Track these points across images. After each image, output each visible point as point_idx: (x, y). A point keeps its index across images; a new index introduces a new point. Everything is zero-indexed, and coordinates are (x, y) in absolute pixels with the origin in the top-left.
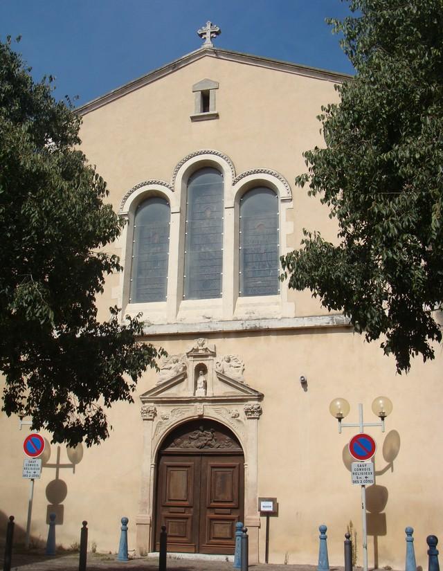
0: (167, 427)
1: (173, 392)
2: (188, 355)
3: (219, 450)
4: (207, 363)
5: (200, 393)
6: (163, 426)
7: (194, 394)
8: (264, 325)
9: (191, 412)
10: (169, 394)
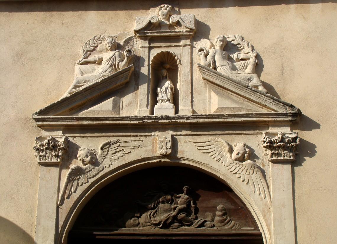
0: (91, 181)
1: (104, 108)
2: (141, 33)
3: (112, 168)
4: (181, 52)
5: (164, 109)
6: (83, 179)
7: (152, 112)
8: (189, 80)
9: (153, 147)
10: (98, 112)
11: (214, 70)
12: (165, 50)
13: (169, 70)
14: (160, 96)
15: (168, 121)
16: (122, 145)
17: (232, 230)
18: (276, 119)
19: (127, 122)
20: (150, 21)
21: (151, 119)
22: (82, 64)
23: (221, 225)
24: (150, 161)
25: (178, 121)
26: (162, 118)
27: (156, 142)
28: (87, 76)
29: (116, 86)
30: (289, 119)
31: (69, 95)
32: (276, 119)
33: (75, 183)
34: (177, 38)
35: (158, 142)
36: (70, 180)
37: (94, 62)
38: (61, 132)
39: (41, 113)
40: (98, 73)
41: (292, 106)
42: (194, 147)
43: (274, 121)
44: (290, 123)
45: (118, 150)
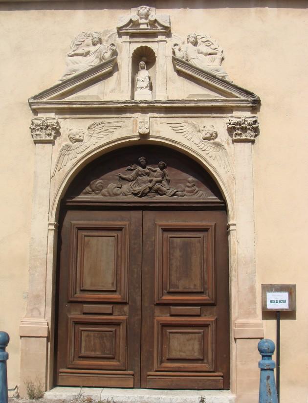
2: (121, 32)
5: (143, 95)
9: (127, 129)
11: (186, 62)
12: (144, 45)
13: (147, 63)
14: (139, 84)
15: (146, 105)
16: (107, 125)
17: (200, 199)
18: (239, 104)
19: (111, 106)
20: (131, 19)
21: (133, 102)
22: (71, 56)
23: (191, 194)
24: (131, 139)
25: (156, 105)
26: (141, 102)
27: (136, 123)
28: (76, 67)
29: (105, 70)
30: (251, 105)
31: (61, 82)
32: (239, 104)
33: (66, 157)
34: (154, 35)
35: (138, 123)
36: (62, 155)
37: (81, 55)
38: (54, 114)
39: (35, 97)
40: (84, 64)
41: (251, 94)
42: (167, 127)
43: (238, 107)
44: (251, 109)
45: (103, 130)
